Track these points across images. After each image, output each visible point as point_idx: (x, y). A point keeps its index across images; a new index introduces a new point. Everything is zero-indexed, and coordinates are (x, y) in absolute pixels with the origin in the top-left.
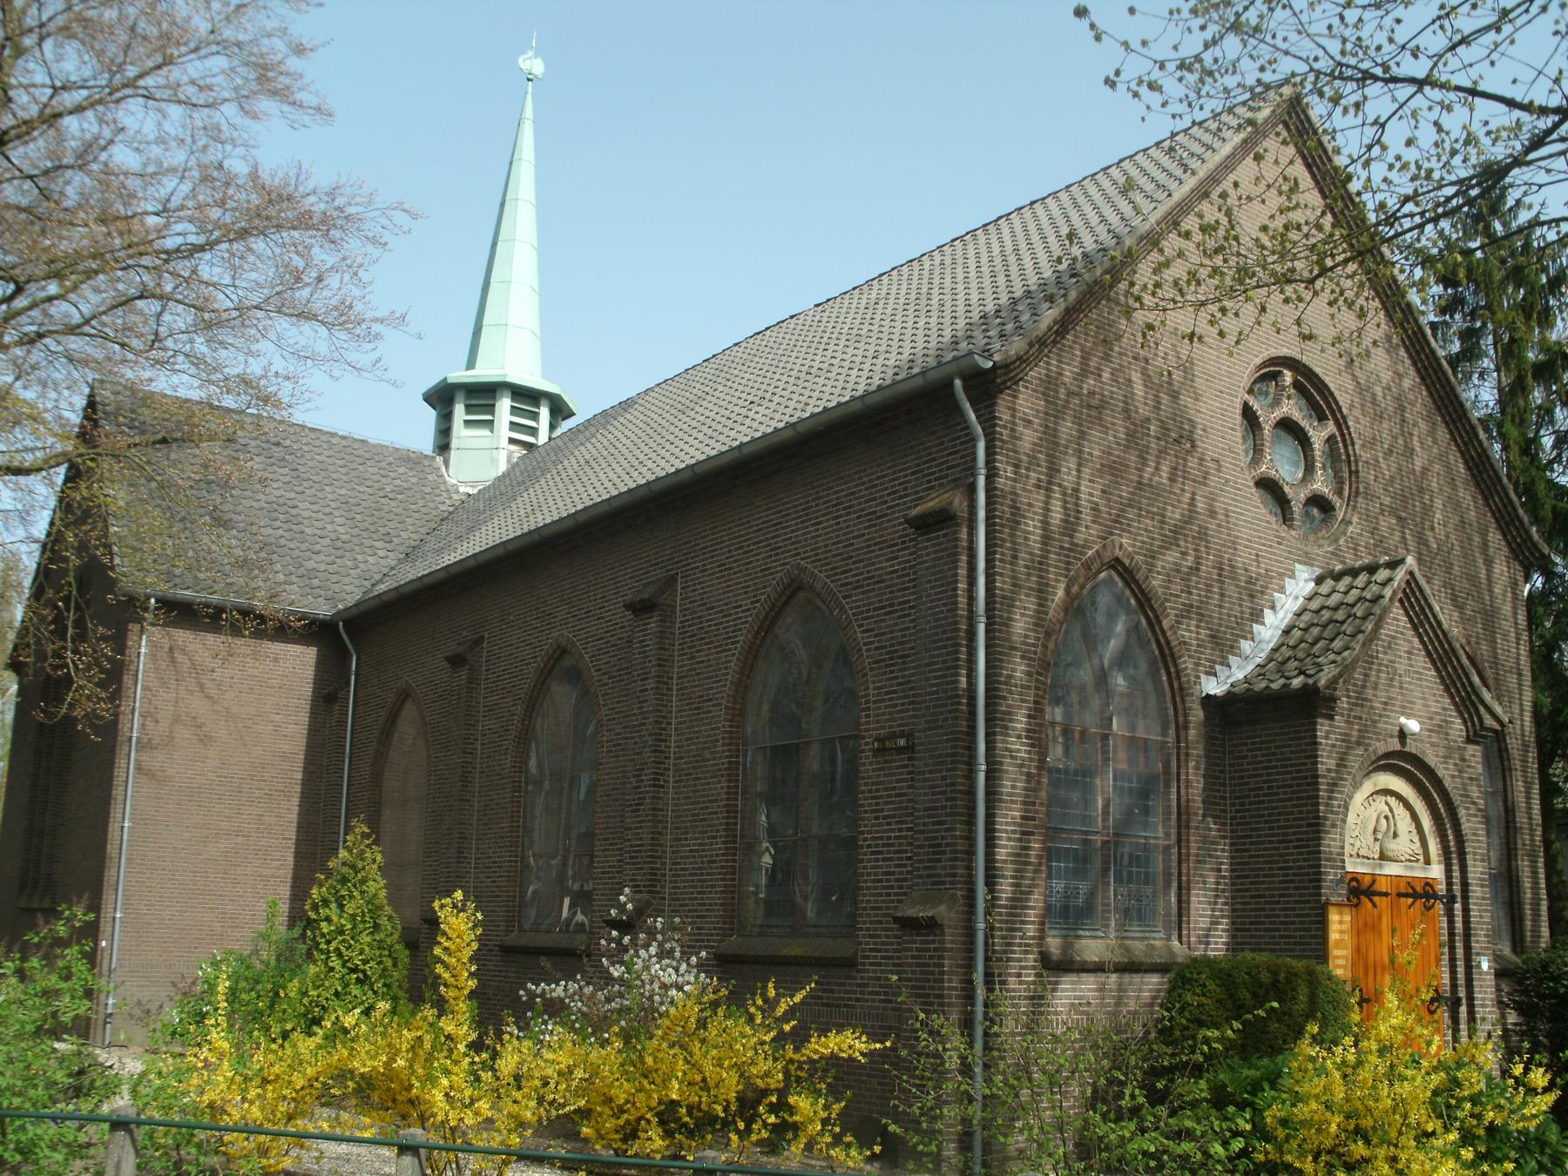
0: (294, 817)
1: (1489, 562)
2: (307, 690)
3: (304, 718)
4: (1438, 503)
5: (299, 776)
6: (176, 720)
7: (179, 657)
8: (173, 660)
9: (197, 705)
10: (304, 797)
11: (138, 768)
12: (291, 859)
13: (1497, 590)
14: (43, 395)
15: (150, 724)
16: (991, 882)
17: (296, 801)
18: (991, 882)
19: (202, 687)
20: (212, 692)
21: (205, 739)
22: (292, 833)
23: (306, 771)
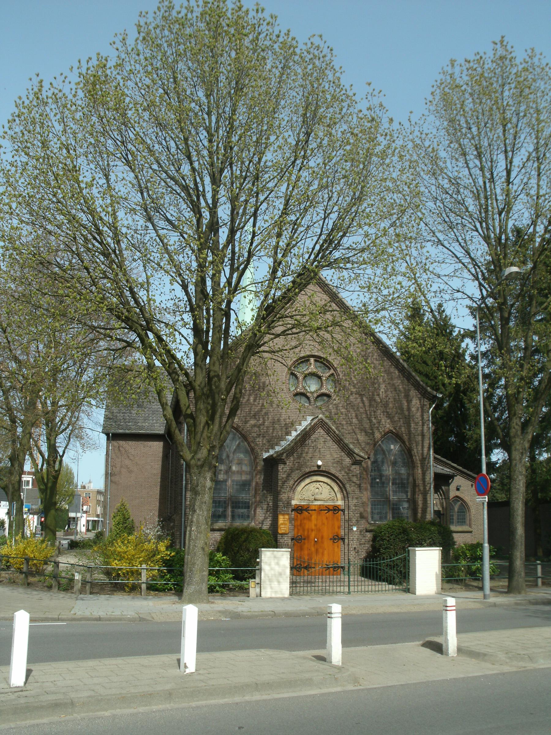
0: (158, 492)
1: (409, 402)
2: (161, 455)
3: (160, 463)
4: (383, 386)
5: (159, 480)
6: (121, 467)
7: (121, 449)
8: (119, 450)
9: (127, 462)
10: (161, 486)
11: (111, 481)
12: (158, 504)
13: (413, 409)
14: (532, 108)
15: (114, 469)
16: (221, 417)
17: (159, 487)
18: (221, 417)
19: (128, 457)
20: (132, 458)
21: (130, 472)
22: (158, 497)
23: (161, 478)
